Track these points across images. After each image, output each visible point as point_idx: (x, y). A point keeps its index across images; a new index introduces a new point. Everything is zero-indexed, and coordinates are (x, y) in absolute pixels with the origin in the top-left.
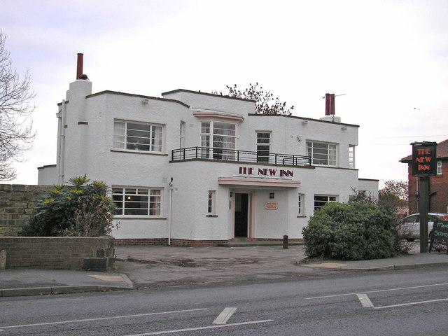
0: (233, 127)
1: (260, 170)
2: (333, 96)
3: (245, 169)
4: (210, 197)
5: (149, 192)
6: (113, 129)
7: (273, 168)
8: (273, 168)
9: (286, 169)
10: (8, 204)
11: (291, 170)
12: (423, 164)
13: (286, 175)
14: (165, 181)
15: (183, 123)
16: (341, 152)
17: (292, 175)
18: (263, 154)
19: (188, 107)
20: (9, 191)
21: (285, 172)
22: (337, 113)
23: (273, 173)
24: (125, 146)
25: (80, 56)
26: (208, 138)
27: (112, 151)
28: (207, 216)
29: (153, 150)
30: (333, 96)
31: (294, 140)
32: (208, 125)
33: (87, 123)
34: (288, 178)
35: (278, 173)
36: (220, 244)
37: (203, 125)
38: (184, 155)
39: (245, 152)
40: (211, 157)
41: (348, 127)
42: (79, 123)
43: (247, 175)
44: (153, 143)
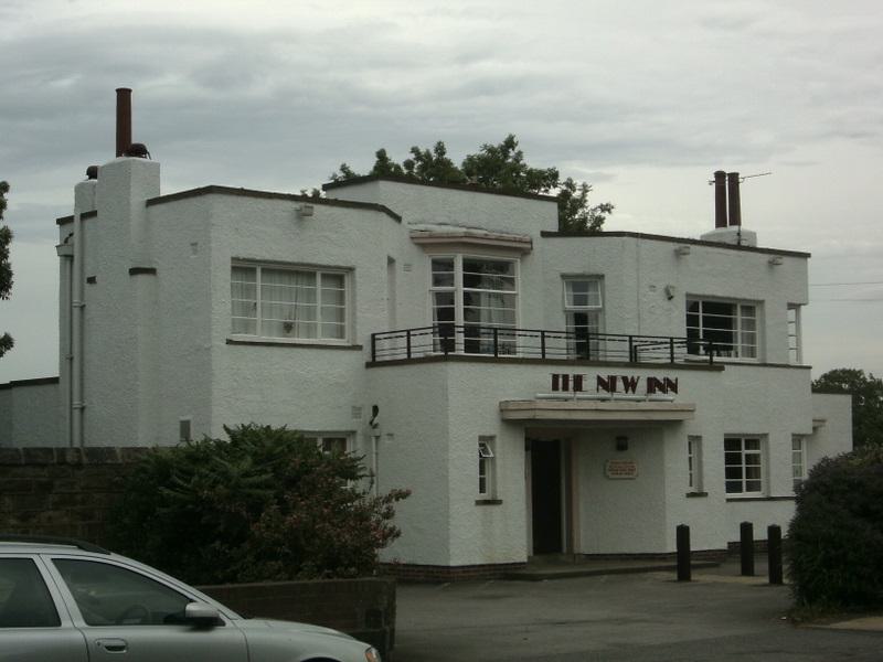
0: (503, 267)
1: (600, 381)
2: (734, 178)
6: (229, 286)
7: (630, 373)
8: (630, 373)
9: (660, 375)
10: (79, 497)
11: (672, 375)
15: (391, 261)
16: (769, 322)
17: (674, 387)
18: (583, 333)
19: (398, 219)
20: (79, 465)
22: (747, 223)
23: (630, 385)
26: (449, 298)
27: (229, 342)
28: (478, 503)
30: (734, 178)
31: (658, 297)
32: (450, 265)
33: (152, 271)
34: (665, 396)
35: (642, 385)
36: (504, 574)
37: (437, 264)
38: (409, 347)
40: (460, 350)
41: (786, 260)
42: (134, 271)
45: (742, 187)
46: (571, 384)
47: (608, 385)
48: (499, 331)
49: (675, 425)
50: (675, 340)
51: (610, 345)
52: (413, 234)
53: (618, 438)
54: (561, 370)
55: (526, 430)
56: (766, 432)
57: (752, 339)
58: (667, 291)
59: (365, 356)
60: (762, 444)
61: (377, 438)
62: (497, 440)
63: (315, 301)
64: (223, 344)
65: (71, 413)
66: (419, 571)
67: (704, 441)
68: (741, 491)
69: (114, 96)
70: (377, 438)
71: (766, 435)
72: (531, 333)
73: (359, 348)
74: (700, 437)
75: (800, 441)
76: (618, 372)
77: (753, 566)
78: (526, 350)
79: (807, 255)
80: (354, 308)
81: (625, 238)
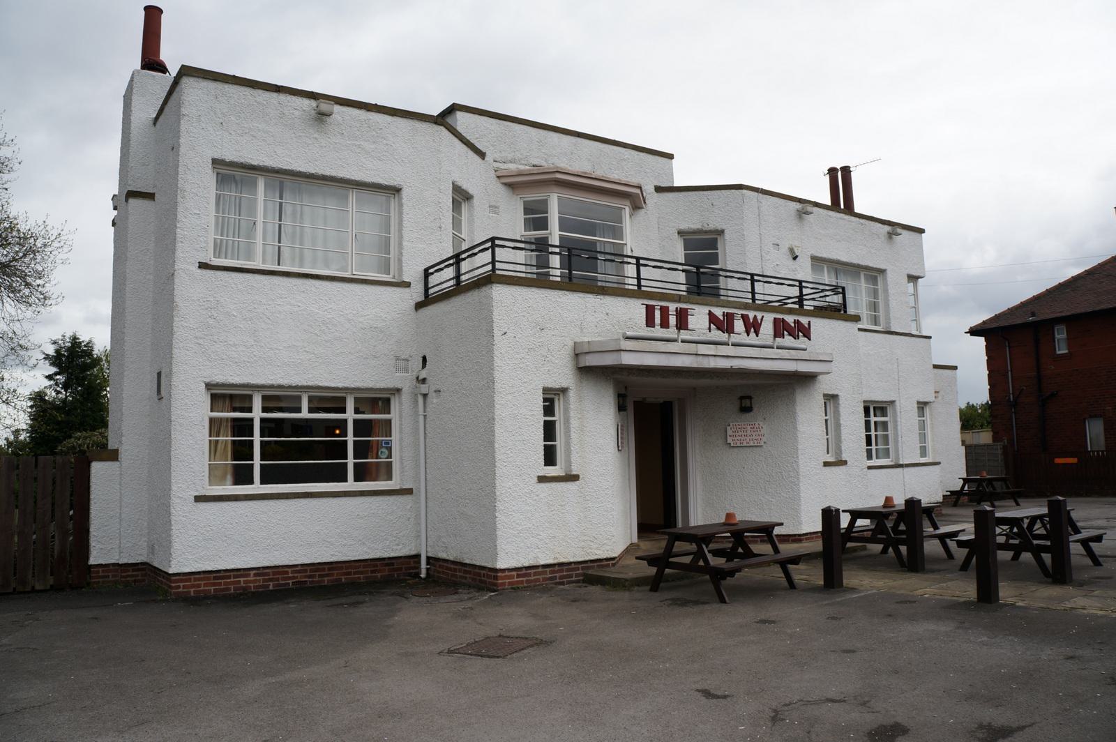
2: (846, 171)
3: (664, 311)
4: (549, 409)
5: (350, 405)
14: (405, 370)
17: (807, 333)
19: (482, 155)
30: (846, 171)
32: (542, 207)
35: (767, 328)
39: (660, 264)
40: (556, 273)
43: (671, 332)
45: (854, 177)
46: (673, 320)
47: (725, 325)
49: (806, 379)
51: (733, 284)
52: (499, 174)
53: (742, 398)
55: (617, 384)
56: (892, 399)
58: (791, 250)
59: (417, 293)
60: (889, 411)
61: (425, 396)
62: (572, 394)
64: (194, 268)
66: (466, 572)
67: (842, 401)
68: (344, 479)
69: (142, 15)
70: (425, 396)
71: (892, 402)
73: (408, 285)
74: (837, 396)
75: (923, 408)
79: (921, 231)
80: (401, 237)
81: (744, 191)
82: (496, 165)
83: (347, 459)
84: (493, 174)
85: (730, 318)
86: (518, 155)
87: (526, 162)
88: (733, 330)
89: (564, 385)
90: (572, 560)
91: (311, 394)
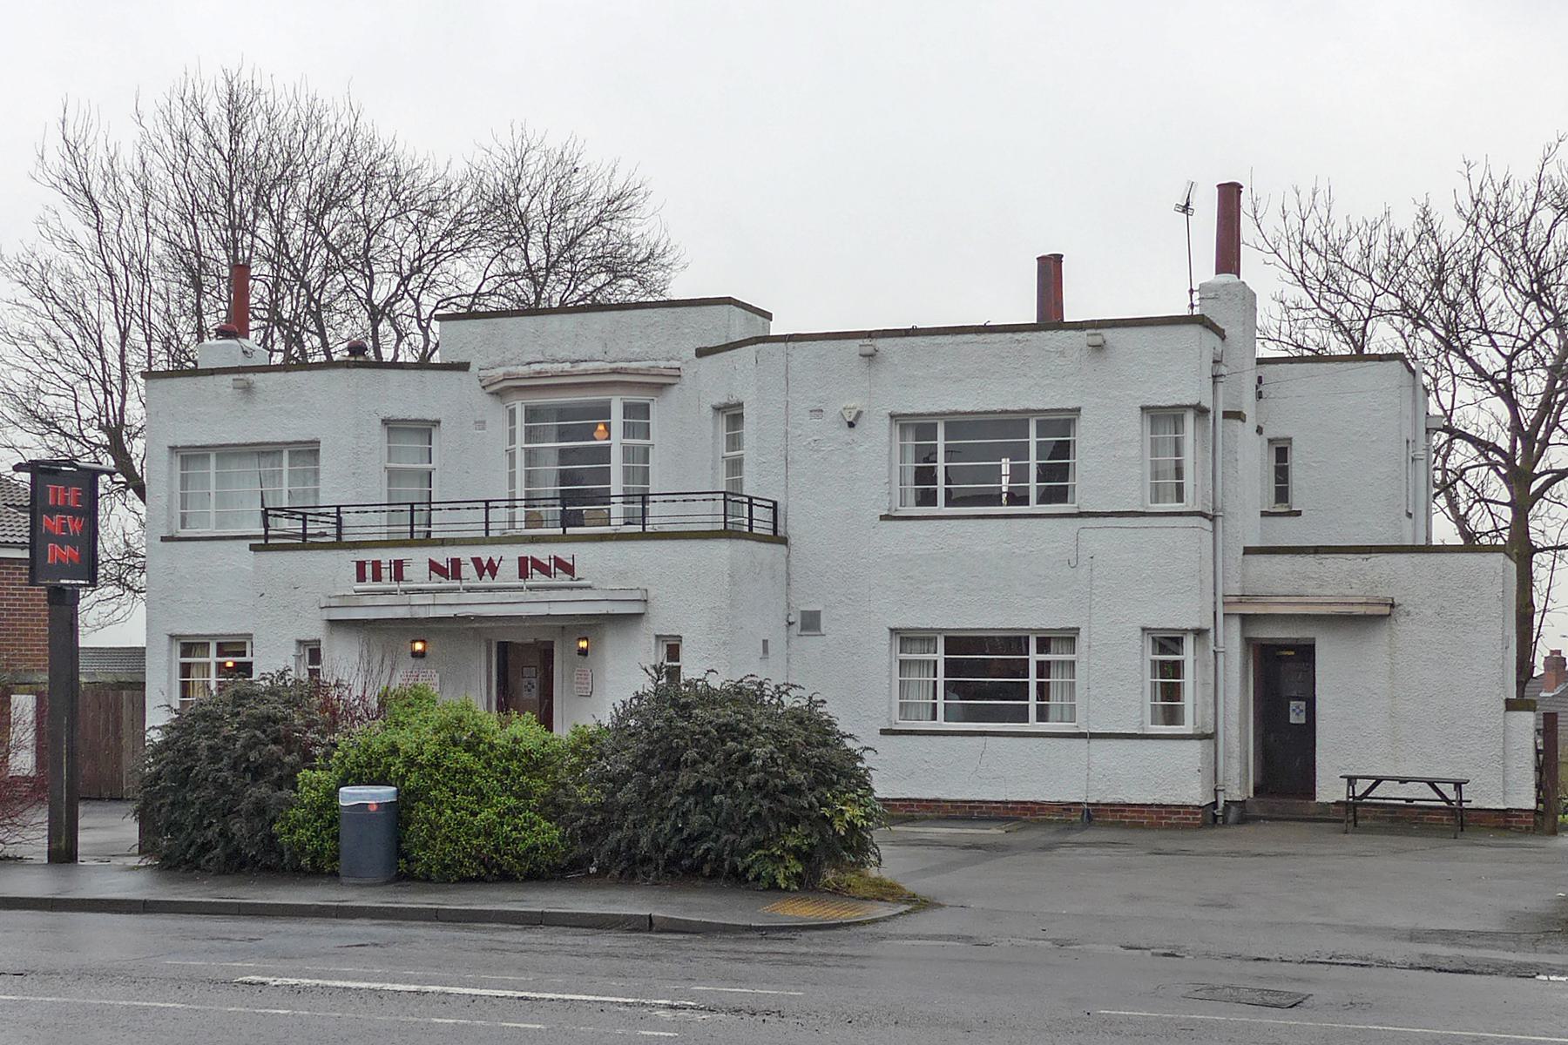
1: (434, 566)
2: (1058, 259)
3: (377, 565)
7: (485, 553)
8: (485, 553)
9: (542, 553)
11: (564, 551)
12: (61, 541)
13: (544, 570)
21: (537, 564)
24: (911, 498)
25: (1230, 195)
29: (1042, 715)
35: (508, 572)
39: (362, 508)
44: (512, 455)
46: (369, 569)
48: (309, 517)
50: (754, 501)
54: (368, 556)
57: (1156, 474)
63: (281, 484)
65: (1216, 658)
72: (469, 505)
76: (465, 554)
77: (77, 836)
78: (442, 527)
82: (482, 373)
83: (1028, 700)
84: (478, 385)
85: (456, 563)
86: (508, 355)
87: (517, 362)
88: (460, 574)
89: (1205, 626)
90: (1009, 799)
91: (1039, 635)
